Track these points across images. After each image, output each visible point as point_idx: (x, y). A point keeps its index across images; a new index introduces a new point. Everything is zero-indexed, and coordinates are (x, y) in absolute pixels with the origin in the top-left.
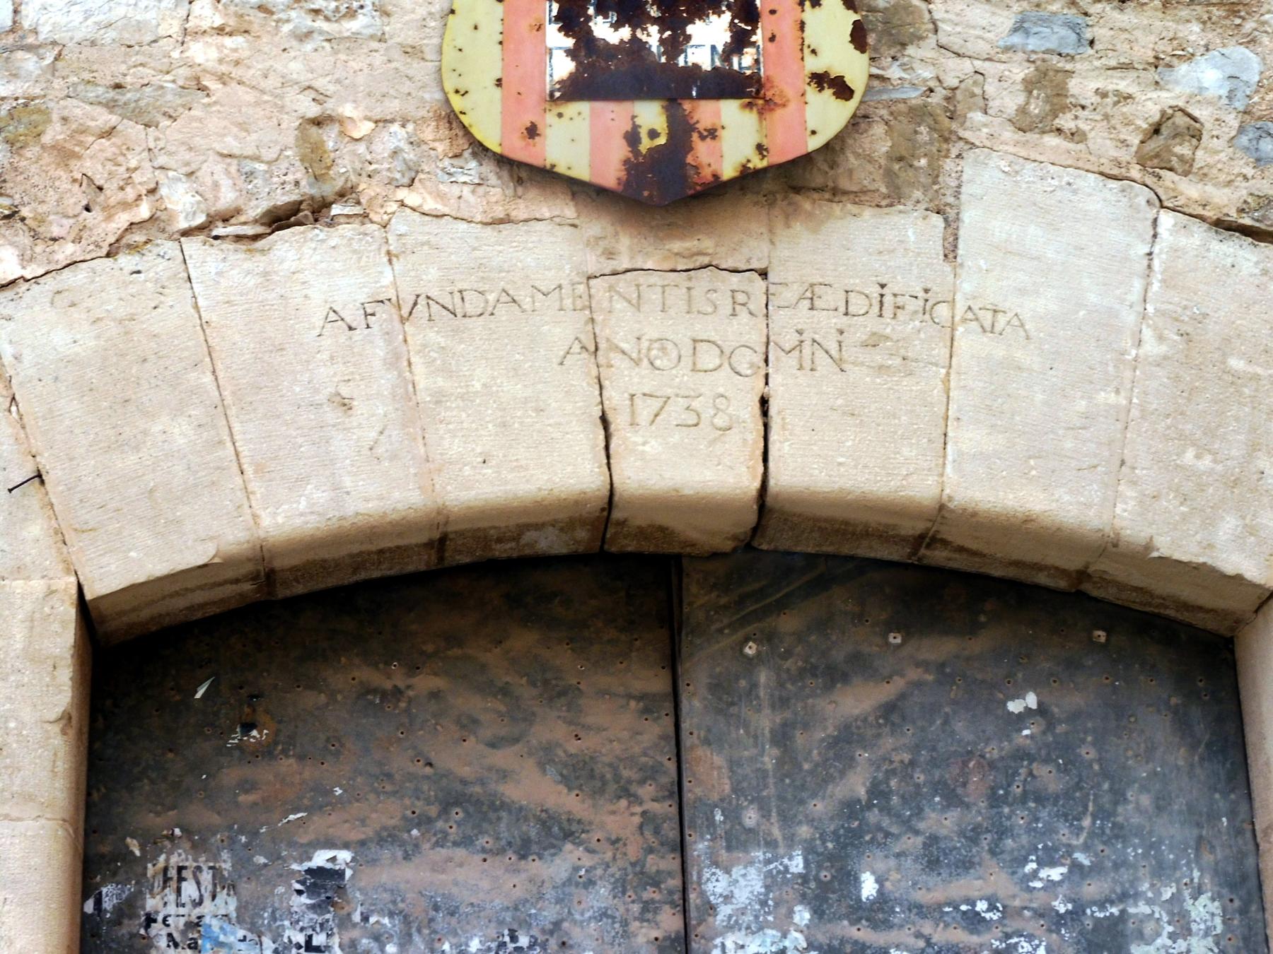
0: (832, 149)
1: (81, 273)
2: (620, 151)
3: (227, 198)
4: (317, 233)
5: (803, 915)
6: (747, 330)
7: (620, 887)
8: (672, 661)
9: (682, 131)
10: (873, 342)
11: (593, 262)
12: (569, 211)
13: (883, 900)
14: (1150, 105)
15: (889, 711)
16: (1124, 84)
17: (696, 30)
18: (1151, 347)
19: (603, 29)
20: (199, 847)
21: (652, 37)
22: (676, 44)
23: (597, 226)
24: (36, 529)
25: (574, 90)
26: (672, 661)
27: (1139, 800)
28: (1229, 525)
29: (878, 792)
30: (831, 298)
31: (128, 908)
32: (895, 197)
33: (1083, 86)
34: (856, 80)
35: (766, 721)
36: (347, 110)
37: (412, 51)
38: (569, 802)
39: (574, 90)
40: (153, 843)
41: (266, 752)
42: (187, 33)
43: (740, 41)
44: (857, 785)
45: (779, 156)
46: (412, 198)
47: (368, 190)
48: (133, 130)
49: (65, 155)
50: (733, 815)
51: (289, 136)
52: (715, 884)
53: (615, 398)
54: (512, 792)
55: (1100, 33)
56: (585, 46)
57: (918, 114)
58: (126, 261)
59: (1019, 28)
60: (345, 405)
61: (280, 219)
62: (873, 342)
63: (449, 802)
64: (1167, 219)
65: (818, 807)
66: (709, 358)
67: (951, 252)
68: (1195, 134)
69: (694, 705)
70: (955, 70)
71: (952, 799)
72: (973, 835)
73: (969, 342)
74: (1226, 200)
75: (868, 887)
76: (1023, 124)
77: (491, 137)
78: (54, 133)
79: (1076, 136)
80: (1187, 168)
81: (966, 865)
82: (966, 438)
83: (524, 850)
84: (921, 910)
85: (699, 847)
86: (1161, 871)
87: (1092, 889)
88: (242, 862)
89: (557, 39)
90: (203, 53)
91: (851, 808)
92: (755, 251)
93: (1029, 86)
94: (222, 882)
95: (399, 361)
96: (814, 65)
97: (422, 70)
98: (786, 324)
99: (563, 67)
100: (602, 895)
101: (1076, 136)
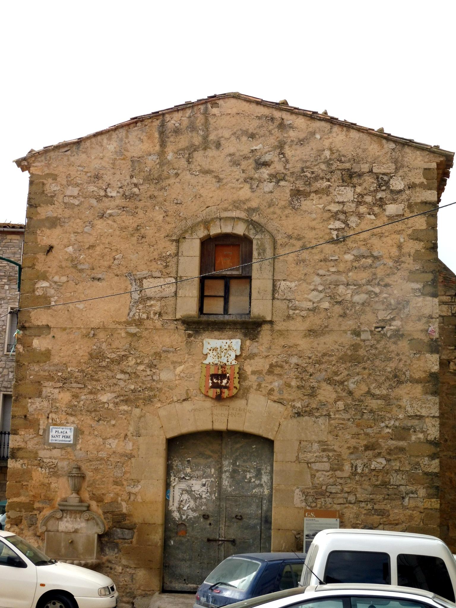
0: (237, 393)
1: (165, 407)
2: (215, 394)
3: (179, 398)
4: (187, 402)
5: (231, 466)
6: (226, 412)
7: (216, 462)
8: (222, 440)
9: (221, 392)
10: (238, 414)
11: (213, 405)
12: (171, 489)
13: (239, 465)
14: (270, 387)
15: (241, 447)
16: (267, 385)
17: (223, 381)
18: (265, 415)
19: (215, 381)
20: (178, 458)
21: (219, 381)
22: (221, 382)
23: (213, 401)
24: (162, 432)
25: (212, 387)
26: (222, 440)
27: (264, 457)
28: (270, 434)
29: (239, 454)
30: (235, 409)
31: (171, 463)
32: (242, 398)
33: (263, 385)
34: (238, 388)
35: (230, 447)
36: (190, 389)
37: (197, 382)
38: (211, 454)
39: (212, 387)
40: (174, 457)
41: (184, 449)
42: (176, 380)
43: (228, 382)
44: (238, 454)
45: (230, 396)
46: (196, 398)
47: (192, 397)
48: (170, 391)
49: (164, 394)
50: (226, 456)
51: (185, 391)
52: (224, 463)
53: (214, 419)
54: (206, 453)
55: (266, 379)
56: (213, 383)
57: (246, 388)
58: (170, 405)
59: (257, 378)
60: (189, 420)
61: (184, 400)
62: (238, 414)
63: (200, 454)
64: (269, 401)
65: (234, 456)
66: (223, 415)
67: (247, 404)
68: (274, 390)
69: (223, 445)
70: (250, 383)
71: (246, 455)
72: (248, 459)
73: (248, 414)
74: (275, 398)
75: (238, 464)
76: (256, 390)
77: (203, 392)
78: (163, 391)
79: (261, 391)
80: (272, 395)
81: (247, 462)
82: (247, 424)
83: (207, 458)
84: (242, 466)
85: (223, 459)
86: (265, 464)
87: (258, 465)
88: (181, 459)
89: (210, 381)
90: (177, 382)
91: (237, 456)
92: (228, 404)
93: (257, 385)
94: (180, 461)
95: (194, 415)
96: (234, 385)
97: (198, 384)
98: (231, 411)
99: (211, 385)
100: (214, 463)
101: (261, 391)
